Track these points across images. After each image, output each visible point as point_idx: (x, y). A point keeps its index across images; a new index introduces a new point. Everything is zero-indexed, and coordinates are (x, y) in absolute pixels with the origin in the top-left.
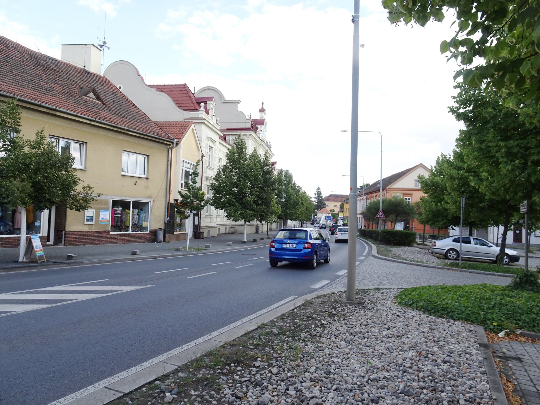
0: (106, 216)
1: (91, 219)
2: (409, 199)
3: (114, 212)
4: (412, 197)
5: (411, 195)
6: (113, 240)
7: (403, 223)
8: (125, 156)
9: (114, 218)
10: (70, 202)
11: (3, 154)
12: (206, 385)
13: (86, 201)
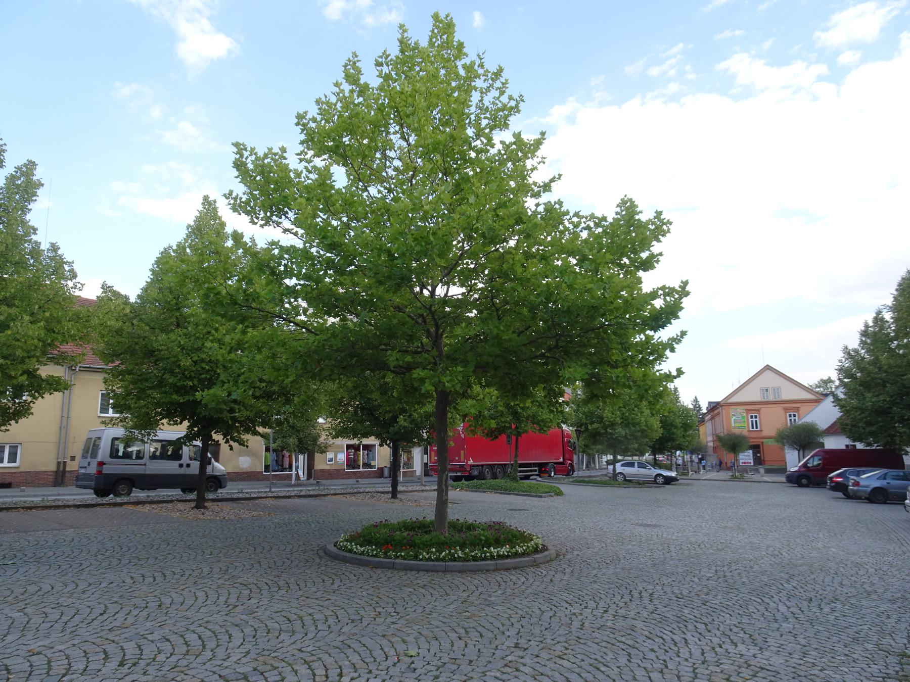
0: (342, 457)
1: (331, 460)
2: (794, 416)
3: (348, 455)
4: (759, 413)
5: (758, 410)
6: (348, 476)
7: (751, 451)
8: (241, 458)
9: (348, 459)
10: (317, 448)
11: (334, 9)
12: (27, 194)
13: (326, 447)
